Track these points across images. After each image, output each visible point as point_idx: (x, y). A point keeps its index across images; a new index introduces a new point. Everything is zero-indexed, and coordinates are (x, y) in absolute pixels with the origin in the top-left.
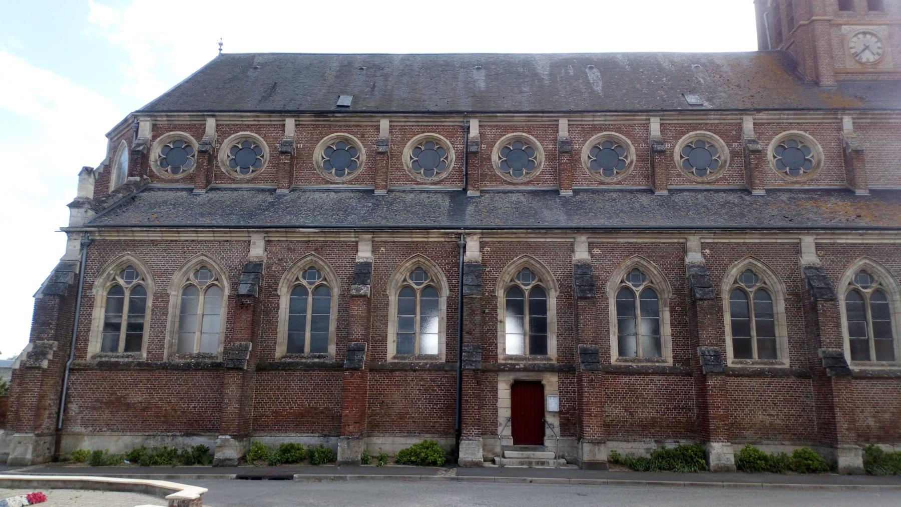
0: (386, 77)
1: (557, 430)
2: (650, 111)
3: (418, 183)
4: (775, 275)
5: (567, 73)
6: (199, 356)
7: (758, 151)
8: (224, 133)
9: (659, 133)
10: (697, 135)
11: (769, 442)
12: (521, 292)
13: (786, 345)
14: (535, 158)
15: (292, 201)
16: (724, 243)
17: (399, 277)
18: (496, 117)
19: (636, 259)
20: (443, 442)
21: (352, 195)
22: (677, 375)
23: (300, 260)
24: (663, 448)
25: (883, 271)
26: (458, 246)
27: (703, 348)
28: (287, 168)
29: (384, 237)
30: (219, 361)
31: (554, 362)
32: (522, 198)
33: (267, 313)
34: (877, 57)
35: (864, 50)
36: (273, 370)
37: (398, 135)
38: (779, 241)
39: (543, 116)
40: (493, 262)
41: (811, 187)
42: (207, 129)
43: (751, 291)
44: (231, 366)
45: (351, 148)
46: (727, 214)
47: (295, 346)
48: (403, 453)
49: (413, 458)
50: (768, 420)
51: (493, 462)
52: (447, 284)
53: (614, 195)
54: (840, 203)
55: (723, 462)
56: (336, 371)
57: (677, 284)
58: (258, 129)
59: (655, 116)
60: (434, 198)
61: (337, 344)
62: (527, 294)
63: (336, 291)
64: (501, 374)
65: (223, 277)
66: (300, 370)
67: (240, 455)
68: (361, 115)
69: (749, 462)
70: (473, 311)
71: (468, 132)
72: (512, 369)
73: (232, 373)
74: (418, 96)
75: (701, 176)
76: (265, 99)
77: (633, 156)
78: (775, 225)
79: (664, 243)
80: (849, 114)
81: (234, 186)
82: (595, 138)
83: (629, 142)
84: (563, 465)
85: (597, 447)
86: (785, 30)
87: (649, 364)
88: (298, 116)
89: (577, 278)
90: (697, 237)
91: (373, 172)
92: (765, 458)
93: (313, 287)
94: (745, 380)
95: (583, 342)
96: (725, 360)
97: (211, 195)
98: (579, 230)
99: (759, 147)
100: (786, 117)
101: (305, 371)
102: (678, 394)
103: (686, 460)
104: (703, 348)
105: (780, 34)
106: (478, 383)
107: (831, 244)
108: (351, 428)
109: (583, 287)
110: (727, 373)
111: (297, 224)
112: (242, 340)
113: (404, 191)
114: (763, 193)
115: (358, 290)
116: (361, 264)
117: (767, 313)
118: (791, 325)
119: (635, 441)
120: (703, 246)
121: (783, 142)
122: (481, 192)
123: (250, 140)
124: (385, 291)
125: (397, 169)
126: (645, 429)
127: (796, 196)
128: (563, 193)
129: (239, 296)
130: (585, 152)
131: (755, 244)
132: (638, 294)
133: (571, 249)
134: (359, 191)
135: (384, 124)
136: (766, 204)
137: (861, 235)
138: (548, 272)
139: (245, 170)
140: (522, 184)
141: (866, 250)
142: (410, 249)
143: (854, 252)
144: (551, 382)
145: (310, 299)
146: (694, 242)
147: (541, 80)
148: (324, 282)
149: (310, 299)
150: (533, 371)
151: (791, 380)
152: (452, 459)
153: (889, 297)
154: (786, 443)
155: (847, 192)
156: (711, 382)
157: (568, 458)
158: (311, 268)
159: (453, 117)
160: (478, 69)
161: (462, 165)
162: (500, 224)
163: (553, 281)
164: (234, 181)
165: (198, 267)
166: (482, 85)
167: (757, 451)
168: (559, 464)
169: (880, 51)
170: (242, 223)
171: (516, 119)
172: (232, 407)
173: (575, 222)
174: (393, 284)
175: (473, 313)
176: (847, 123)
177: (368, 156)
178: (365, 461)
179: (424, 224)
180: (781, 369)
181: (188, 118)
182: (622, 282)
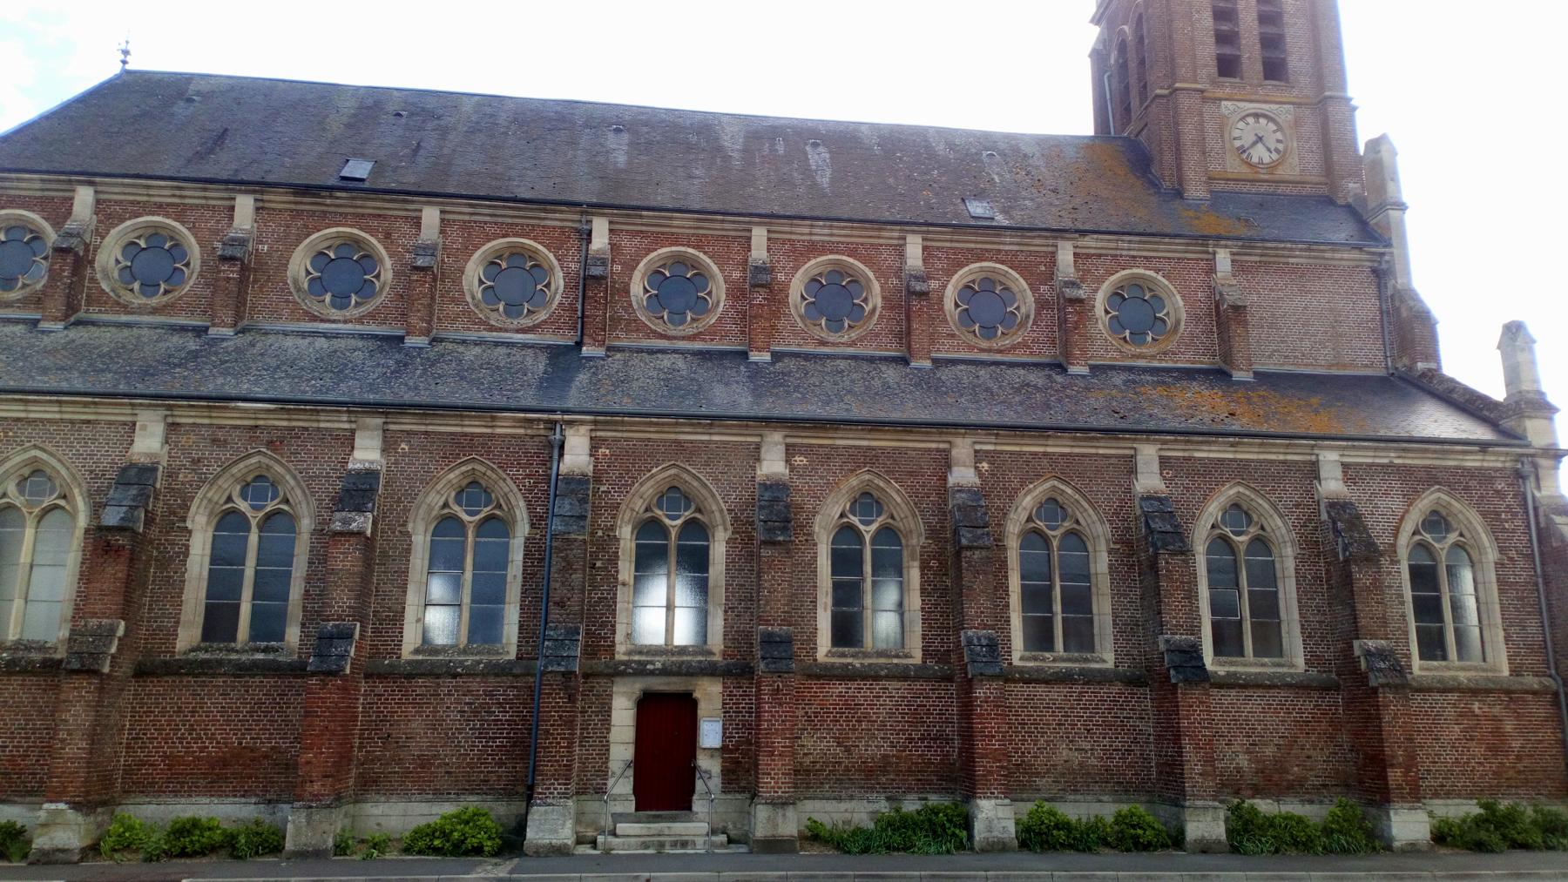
0: (444, 132)
1: (716, 783)
2: (907, 223)
3: (492, 329)
4: (1094, 509)
5: (772, 150)
6: (18, 645)
7: (1080, 301)
8: (109, 216)
9: (920, 263)
10: (982, 270)
11: (1078, 797)
12: (664, 532)
13: (1109, 630)
14: (710, 294)
15: (238, 350)
16: (1012, 453)
17: (216, 494)
18: (641, 217)
19: (867, 477)
20: (502, 810)
21: (360, 344)
22: (928, 679)
23: (236, 463)
24: (897, 810)
25: (1266, 506)
26: (550, 445)
27: (970, 633)
28: (233, 287)
29: (408, 424)
30: (58, 656)
31: (718, 658)
32: (680, 363)
33: (165, 562)
34: (1275, 156)
35: (1255, 143)
36: (168, 674)
37: (456, 238)
38: (1101, 451)
39: (724, 220)
40: (614, 474)
41: (1164, 365)
42: (77, 208)
43: (1055, 535)
44: (76, 665)
45: (34, 238)
46: (1021, 403)
47: (218, 621)
48: (418, 834)
49: (436, 842)
50: (1077, 757)
51: (594, 844)
52: (525, 515)
53: (842, 364)
54: (1206, 393)
55: (995, 834)
56: (296, 677)
57: (934, 520)
58: (180, 213)
59: (914, 232)
60: (518, 355)
61: (303, 625)
62: (673, 534)
63: (306, 524)
64: (617, 679)
65: (76, 491)
66: (224, 674)
67: (87, 842)
68: (390, 196)
69: (1040, 834)
70: (570, 564)
71: (589, 241)
72: (641, 671)
73: (77, 681)
74: (499, 169)
75: (989, 339)
76: (200, 156)
77: (876, 300)
78: (1095, 424)
79: (915, 449)
80: (1226, 247)
81: (124, 318)
82: (813, 265)
83: (871, 275)
84: (722, 846)
85: (780, 812)
86: (1135, 103)
87: (882, 661)
88: (262, 193)
89: (761, 508)
90: (969, 440)
91: (404, 300)
92: (1065, 826)
93: (261, 514)
94: (1041, 689)
95: (767, 622)
96: (1009, 653)
97: (73, 334)
98: (769, 422)
99: (1081, 293)
100: (1126, 246)
101: (235, 676)
102: (929, 713)
103: (935, 832)
104: (970, 633)
105: (1128, 110)
106: (571, 699)
107: (1185, 458)
108: (316, 787)
109: (773, 522)
110: (1009, 676)
111: (234, 392)
112: (104, 615)
113: (464, 342)
114: (1085, 370)
115: (345, 522)
116: (358, 473)
117: (1080, 574)
118: (1117, 594)
119: (851, 798)
120: (979, 456)
121: (1122, 288)
122: (609, 349)
123: (164, 233)
124: (404, 524)
125: (453, 300)
126: (869, 776)
127: (1137, 378)
128: (755, 357)
129: (100, 528)
130: (797, 286)
131: (1063, 455)
132: (868, 538)
133: (755, 454)
134: (375, 337)
135: (431, 216)
136: (1087, 389)
137: (1232, 445)
138: (713, 496)
139: (149, 287)
140: (683, 338)
141: (1241, 471)
142: (460, 446)
143: (1222, 474)
144: (710, 694)
145: (253, 538)
146: (963, 448)
147: (727, 158)
148: (285, 507)
149: (253, 538)
150: (678, 674)
151: (1115, 689)
152: (511, 842)
153: (1275, 550)
154: (1105, 798)
155: (1219, 375)
156: (980, 693)
157: (733, 833)
158: (259, 478)
159: (562, 212)
160: (618, 131)
161: (576, 299)
162: (631, 408)
163: (721, 511)
164: (126, 308)
165: (26, 471)
166: (621, 159)
167: (1054, 815)
168: (713, 845)
169: (1280, 147)
170: (122, 388)
171: (675, 223)
172: (75, 748)
173: (766, 408)
174: (421, 511)
175: (568, 567)
176: (1223, 260)
177: (397, 274)
178: (341, 848)
179: (488, 403)
180: (1099, 670)
181: (38, 185)
182: (842, 515)
